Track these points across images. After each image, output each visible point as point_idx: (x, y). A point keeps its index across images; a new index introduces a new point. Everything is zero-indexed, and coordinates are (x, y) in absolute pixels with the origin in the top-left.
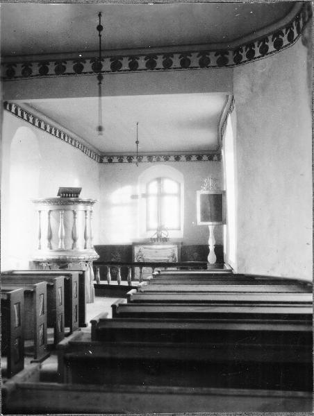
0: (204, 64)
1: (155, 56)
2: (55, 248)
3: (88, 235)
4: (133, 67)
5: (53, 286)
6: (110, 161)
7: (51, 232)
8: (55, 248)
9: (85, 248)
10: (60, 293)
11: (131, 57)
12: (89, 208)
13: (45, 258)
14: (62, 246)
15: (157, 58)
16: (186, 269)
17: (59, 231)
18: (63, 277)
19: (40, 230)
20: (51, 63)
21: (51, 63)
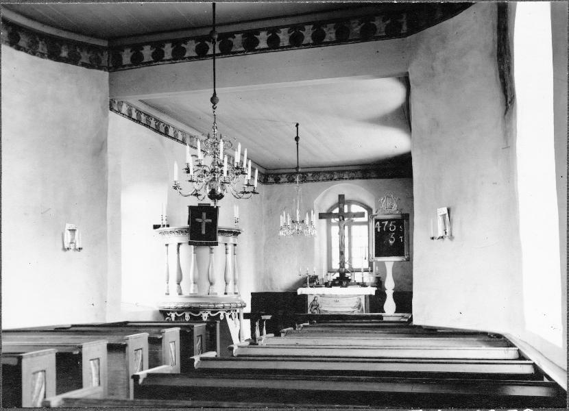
0: (318, 41)
1: (301, 27)
2: (186, 293)
3: (230, 276)
4: (179, 55)
5: (161, 339)
6: (277, 181)
7: (181, 275)
8: (186, 293)
9: (226, 294)
10: (172, 350)
11: (269, 30)
12: (231, 239)
13: (173, 306)
14: (194, 290)
15: (143, 49)
16: (378, 315)
17: (189, 273)
18: (179, 329)
19: (168, 273)
20: (307, 27)
21: (307, 27)
